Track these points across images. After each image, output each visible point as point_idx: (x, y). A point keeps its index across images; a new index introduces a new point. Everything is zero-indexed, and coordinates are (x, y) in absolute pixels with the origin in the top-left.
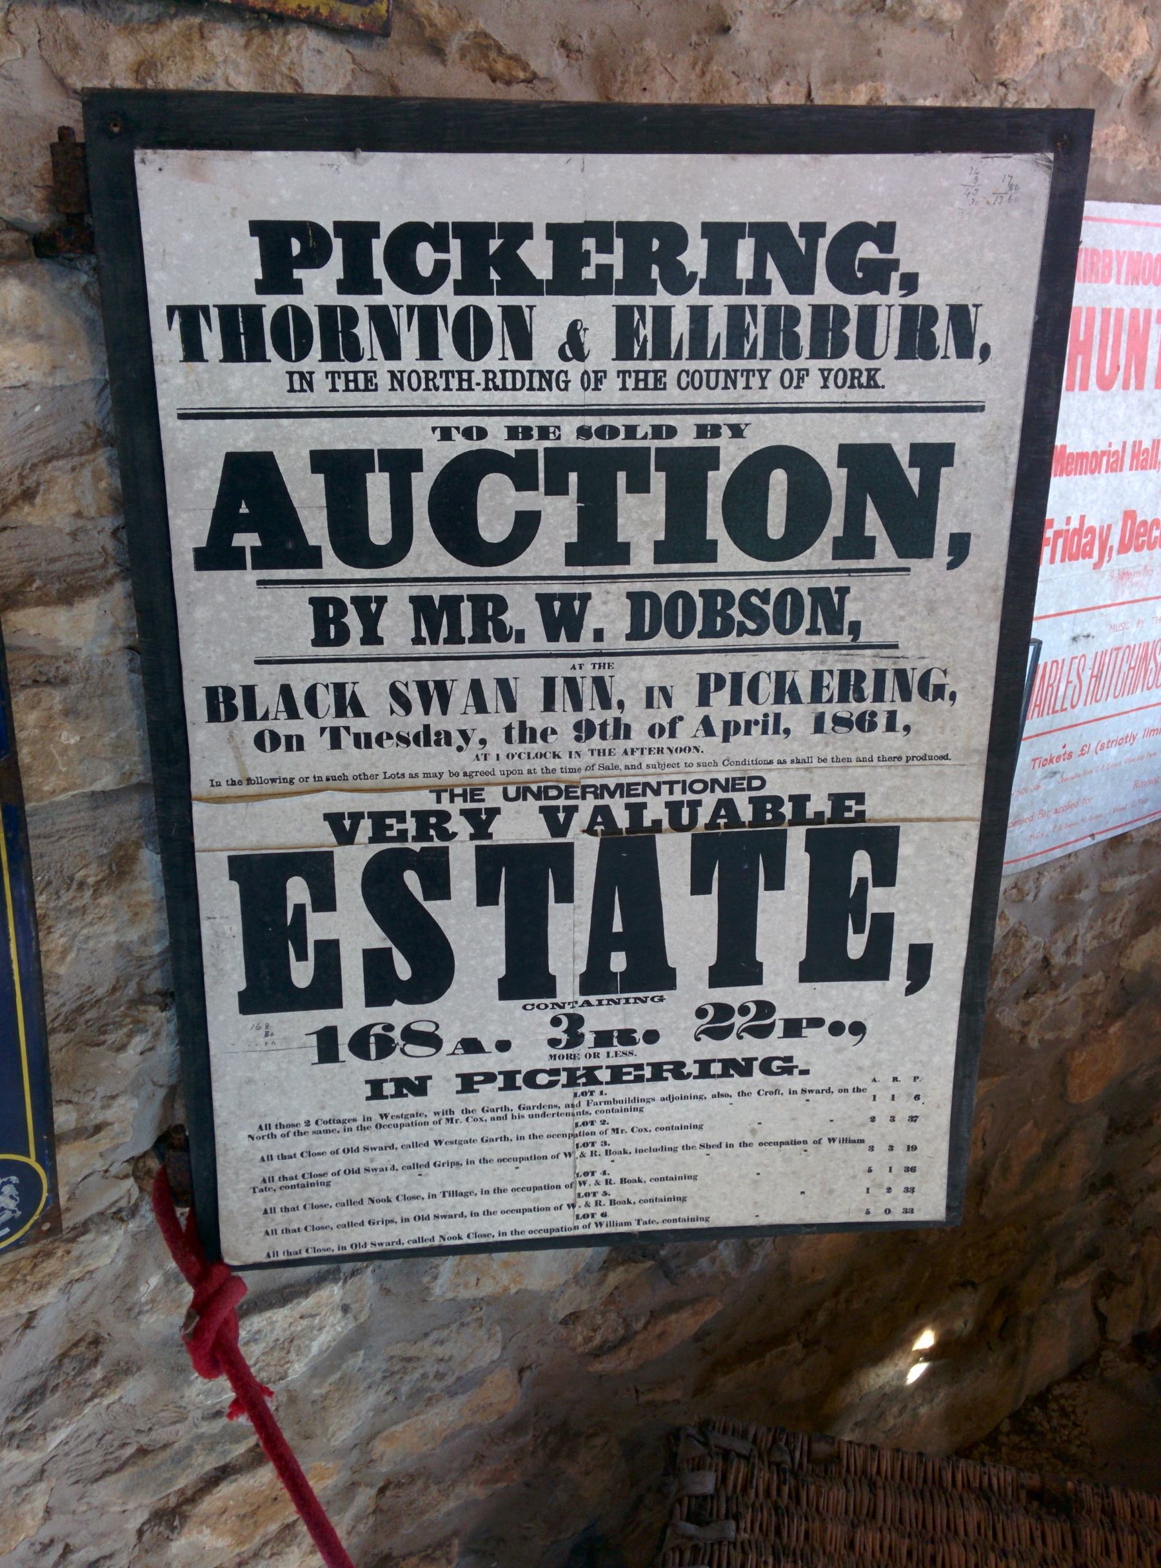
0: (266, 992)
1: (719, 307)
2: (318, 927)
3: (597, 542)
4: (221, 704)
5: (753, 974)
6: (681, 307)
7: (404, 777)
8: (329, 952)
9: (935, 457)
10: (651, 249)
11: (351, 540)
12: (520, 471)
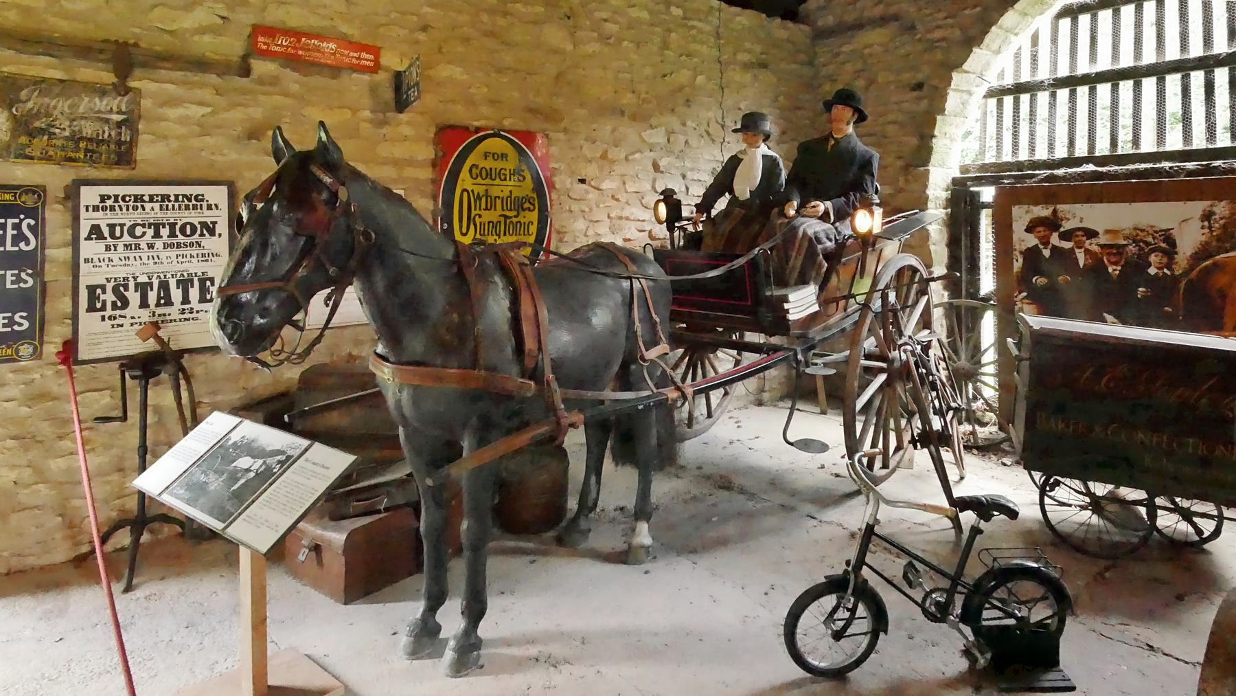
0: (91, 308)
1: (176, 205)
2: (102, 297)
3: (157, 235)
4: (86, 261)
5: (189, 303)
6: (170, 205)
7: (121, 273)
8: (104, 302)
9: (214, 223)
10: (165, 198)
11: (113, 236)
12: (143, 226)
